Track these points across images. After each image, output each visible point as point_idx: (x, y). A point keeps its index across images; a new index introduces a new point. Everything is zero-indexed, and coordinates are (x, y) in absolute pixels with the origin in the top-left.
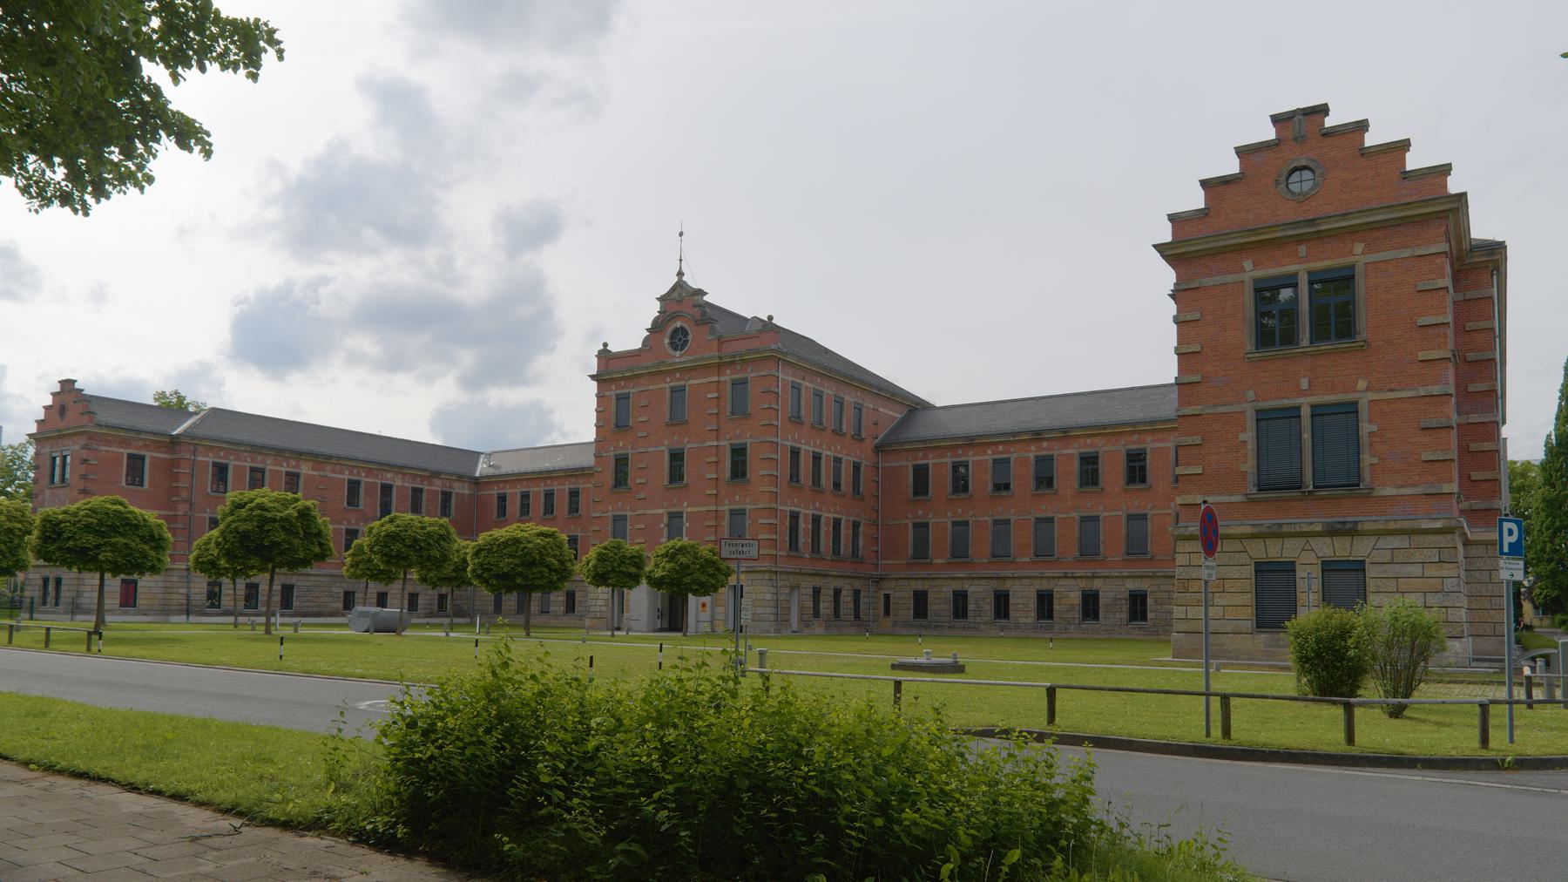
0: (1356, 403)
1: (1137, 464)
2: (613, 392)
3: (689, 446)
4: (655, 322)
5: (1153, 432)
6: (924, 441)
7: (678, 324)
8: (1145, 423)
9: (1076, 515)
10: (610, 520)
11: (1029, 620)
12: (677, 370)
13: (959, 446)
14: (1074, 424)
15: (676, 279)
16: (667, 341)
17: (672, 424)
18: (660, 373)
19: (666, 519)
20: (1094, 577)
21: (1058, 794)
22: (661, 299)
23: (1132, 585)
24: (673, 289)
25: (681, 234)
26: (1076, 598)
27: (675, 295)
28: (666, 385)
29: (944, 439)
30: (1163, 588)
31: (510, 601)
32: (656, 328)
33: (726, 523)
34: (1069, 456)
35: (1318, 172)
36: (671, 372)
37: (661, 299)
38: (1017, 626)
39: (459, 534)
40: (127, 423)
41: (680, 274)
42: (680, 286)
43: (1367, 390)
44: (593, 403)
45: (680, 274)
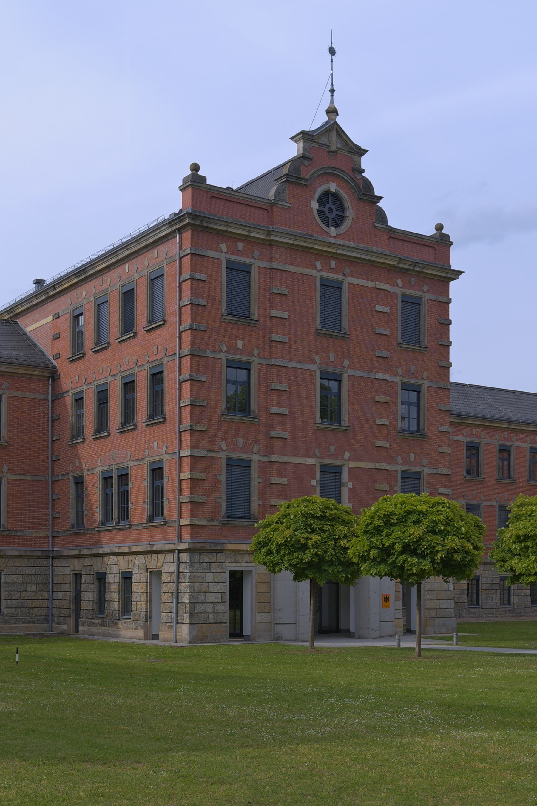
2: (222, 253)
7: (333, 187)
28: (318, 272)
41: (332, 112)
43: (350, 459)
45: (332, 112)
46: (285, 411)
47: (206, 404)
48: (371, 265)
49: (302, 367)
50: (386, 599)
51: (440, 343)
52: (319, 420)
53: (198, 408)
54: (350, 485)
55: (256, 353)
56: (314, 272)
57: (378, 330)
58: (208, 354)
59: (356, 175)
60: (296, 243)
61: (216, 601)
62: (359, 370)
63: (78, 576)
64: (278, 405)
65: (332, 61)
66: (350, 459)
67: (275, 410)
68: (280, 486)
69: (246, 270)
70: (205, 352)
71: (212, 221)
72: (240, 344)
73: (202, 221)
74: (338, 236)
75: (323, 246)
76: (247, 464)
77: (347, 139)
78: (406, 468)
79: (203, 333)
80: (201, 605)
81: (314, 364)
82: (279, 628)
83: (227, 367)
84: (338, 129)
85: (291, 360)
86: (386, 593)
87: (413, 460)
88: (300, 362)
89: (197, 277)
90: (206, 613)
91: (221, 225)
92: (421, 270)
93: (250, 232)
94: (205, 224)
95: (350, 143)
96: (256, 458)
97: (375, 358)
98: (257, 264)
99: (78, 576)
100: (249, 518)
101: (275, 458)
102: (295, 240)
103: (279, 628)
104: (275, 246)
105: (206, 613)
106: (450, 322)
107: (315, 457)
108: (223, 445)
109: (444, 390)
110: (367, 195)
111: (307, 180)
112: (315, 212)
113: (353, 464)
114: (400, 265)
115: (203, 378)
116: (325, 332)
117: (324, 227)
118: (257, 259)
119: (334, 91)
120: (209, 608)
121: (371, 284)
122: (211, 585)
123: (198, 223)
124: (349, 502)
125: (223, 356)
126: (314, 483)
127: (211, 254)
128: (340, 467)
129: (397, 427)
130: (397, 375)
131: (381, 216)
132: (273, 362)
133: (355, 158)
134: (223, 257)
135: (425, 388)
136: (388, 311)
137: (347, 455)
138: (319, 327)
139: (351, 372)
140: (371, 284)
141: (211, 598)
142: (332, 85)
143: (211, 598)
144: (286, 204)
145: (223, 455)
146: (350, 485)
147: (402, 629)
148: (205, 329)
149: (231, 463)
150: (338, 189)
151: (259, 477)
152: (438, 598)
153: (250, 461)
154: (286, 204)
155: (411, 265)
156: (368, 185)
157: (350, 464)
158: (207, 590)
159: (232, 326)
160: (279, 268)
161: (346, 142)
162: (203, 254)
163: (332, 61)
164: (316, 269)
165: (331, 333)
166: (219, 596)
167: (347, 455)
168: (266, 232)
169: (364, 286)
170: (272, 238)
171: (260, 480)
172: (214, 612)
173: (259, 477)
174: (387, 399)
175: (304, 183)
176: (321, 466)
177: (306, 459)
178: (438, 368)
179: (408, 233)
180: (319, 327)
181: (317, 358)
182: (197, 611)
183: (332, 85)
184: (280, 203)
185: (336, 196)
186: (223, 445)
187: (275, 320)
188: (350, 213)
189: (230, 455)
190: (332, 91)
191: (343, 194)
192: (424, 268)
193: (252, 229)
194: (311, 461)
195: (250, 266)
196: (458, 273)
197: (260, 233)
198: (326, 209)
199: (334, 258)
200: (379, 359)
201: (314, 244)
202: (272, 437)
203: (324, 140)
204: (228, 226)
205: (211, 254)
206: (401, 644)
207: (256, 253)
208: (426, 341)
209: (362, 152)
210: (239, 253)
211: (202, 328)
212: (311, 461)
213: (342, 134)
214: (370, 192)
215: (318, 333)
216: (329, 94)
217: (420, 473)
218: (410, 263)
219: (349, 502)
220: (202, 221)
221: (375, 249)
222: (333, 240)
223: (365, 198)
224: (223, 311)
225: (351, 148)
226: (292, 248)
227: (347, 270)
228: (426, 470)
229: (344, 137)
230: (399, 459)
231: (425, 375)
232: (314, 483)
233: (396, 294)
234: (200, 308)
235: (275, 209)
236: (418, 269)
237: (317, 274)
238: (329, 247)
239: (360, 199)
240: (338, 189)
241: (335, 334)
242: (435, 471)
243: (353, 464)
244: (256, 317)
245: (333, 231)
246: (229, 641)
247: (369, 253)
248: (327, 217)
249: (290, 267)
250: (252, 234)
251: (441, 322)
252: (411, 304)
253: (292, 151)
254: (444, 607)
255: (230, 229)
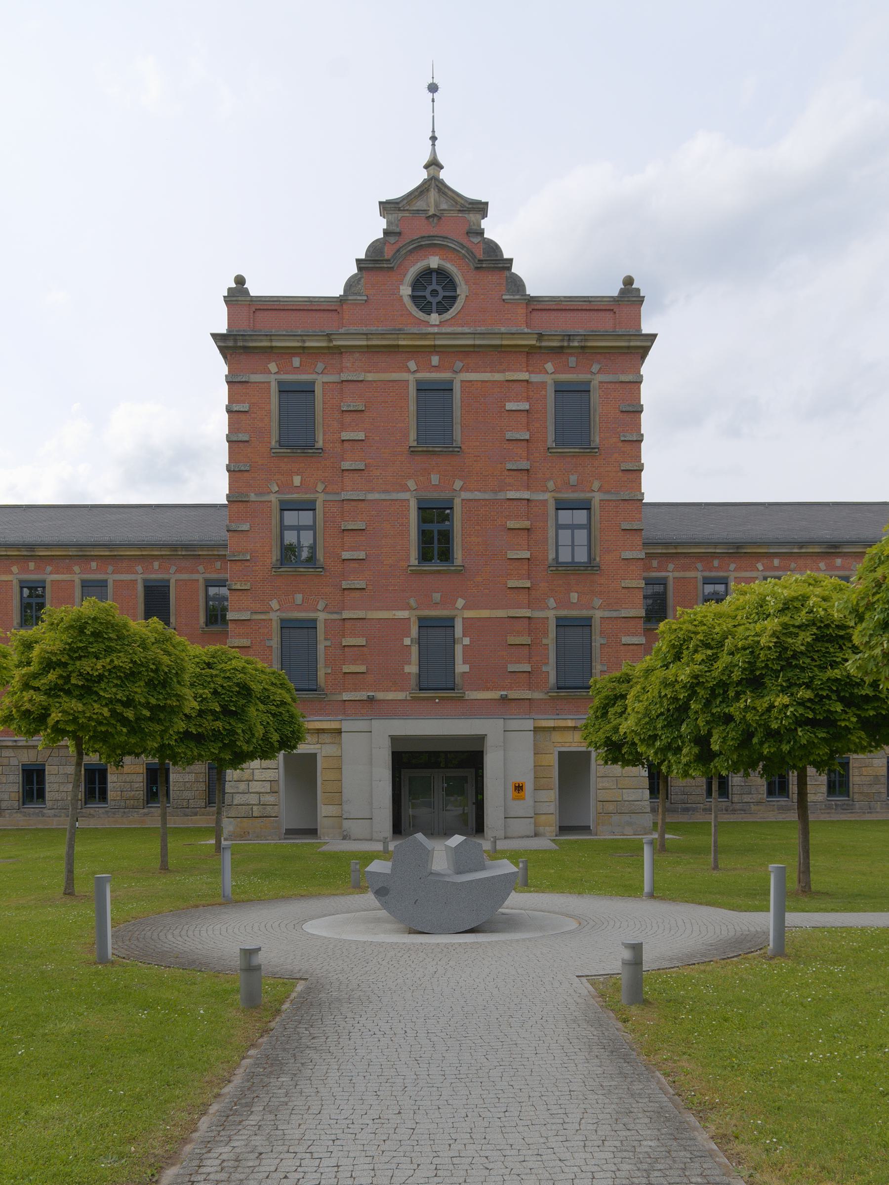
0: (590, 618)
2: (272, 375)
3: (463, 496)
4: (375, 248)
6: (666, 544)
7: (434, 262)
10: (275, 626)
12: (434, 349)
13: (714, 555)
14: (847, 537)
15: (424, 175)
16: (406, 291)
18: (394, 349)
19: (414, 631)
22: (386, 207)
24: (421, 191)
25: (433, 88)
27: (420, 204)
28: (411, 374)
29: (698, 544)
31: (127, 776)
32: (374, 263)
33: (550, 640)
36: (415, 351)
37: (386, 207)
41: (434, 164)
42: (433, 184)
43: (465, 608)
44: (222, 394)
45: (434, 164)
46: (362, 555)
47: (248, 558)
48: (499, 352)
49: (387, 498)
50: (519, 788)
51: (622, 439)
52: (414, 561)
53: (239, 564)
54: (407, 641)
55: (320, 487)
56: (404, 376)
57: (509, 435)
58: (253, 497)
59: (472, 239)
60: (370, 343)
61: (263, 790)
62: (480, 491)
65: (433, 101)
66: (465, 608)
67: (346, 555)
68: (356, 649)
69: (308, 390)
70: (247, 496)
71: (247, 338)
72: (297, 480)
73: (235, 340)
74: (442, 324)
75: (412, 339)
76: (310, 625)
77: (454, 195)
78: (563, 613)
79: (245, 474)
80: (241, 795)
81: (407, 491)
82: (346, 824)
83: (557, 509)
84: (440, 185)
85: (372, 490)
86: (519, 780)
87: (575, 601)
88: (385, 491)
89: (235, 409)
90: (248, 805)
91: (261, 341)
92: (583, 344)
93: (304, 341)
94: (240, 344)
95: (459, 199)
96: (322, 616)
97: (507, 473)
98: (321, 378)
100: (454, 689)
101: (346, 615)
102: (368, 339)
103: (346, 824)
104: (346, 352)
105: (248, 805)
106: (639, 410)
107: (409, 608)
108: (275, 604)
109: (631, 502)
110: (494, 262)
111: (389, 260)
112: (408, 301)
113: (469, 614)
114: (544, 344)
115: (245, 527)
116: (420, 449)
117: (421, 315)
118: (322, 373)
119: (430, 138)
120: (253, 799)
121: (498, 377)
122: (256, 771)
123: (231, 344)
124: (464, 663)
125: (273, 498)
126: (407, 641)
127: (255, 378)
128: (452, 619)
129: (547, 560)
130: (546, 490)
131: (517, 284)
132: (344, 496)
133: (472, 217)
134: (549, 379)
135: (596, 504)
136: (527, 407)
137: (460, 603)
138: (415, 444)
139: (465, 495)
140: (498, 377)
141: (255, 787)
142: (433, 131)
143: (255, 787)
144: (359, 298)
145: (274, 616)
146: (467, 641)
147: (553, 828)
148: (247, 468)
149: (287, 625)
150: (442, 262)
151: (326, 639)
152: (619, 786)
153: (315, 621)
154: (359, 298)
155: (563, 340)
156: (493, 248)
157: (463, 612)
158: (251, 778)
159: (285, 460)
160: (350, 378)
161: (453, 199)
162: (243, 380)
163: (433, 101)
164: (409, 371)
165: (431, 449)
166: (268, 785)
167: (460, 603)
168: (326, 338)
169: (487, 382)
170: (335, 343)
171: (328, 643)
172: (259, 804)
173: (326, 639)
174: (526, 524)
175: (385, 266)
176: (421, 619)
177: (394, 612)
178: (620, 474)
179: (563, 299)
180: (415, 444)
181: (411, 484)
182: (235, 802)
183: (433, 131)
184: (350, 298)
185: (441, 273)
186: (275, 604)
187: (346, 444)
188: (462, 290)
189: (284, 615)
190: (434, 138)
192: (586, 340)
193: (305, 338)
196: (653, 337)
197: (359, 339)
199: (437, 353)
200: (512, 473)
201: (398, 339)
202: (344, 589)
203: (420, 204)
204: (271, 340)
205: (255, 378)
206: (213, 842)
208: (597, 440)
209: (481, 208)
210: (296, 370)
211: (243, 468)
213: (446, 190)
214: (497, 256)
215: (413, 452)
216: (430, 142)
217: (590, 618)
218: (560, 338)
219: (464, 663)
220: (235, 340)
221: (503, 330)
222: (436, 330)
223: (484, 265)
224: (273, 443)
225: (462, 206)
226: (370, 350)
227: (459, 365)
228: (598, 614)
229: (450, 193)
230: (552, 602)
231: (596, 485)
233: (543, 384)
234: (241, 445)
235: (345, 307)
236: (576, 344)
237: (411, 378)
238: (421, 339)
239: (477, 268)
240: (442, 262)
241: (437, 449)
242: (615, 614)
243: (469, 614)
244: (320, 444)
245: (434, 318)
246: (285, 839)
247: (515, 336)
248: (429, 302)
249: (368, 374)
250: (307, 344)
251: (624, 410)
252: (573, 394)
253: (376, 227)
254: (631, 799)
255: (274, 344)
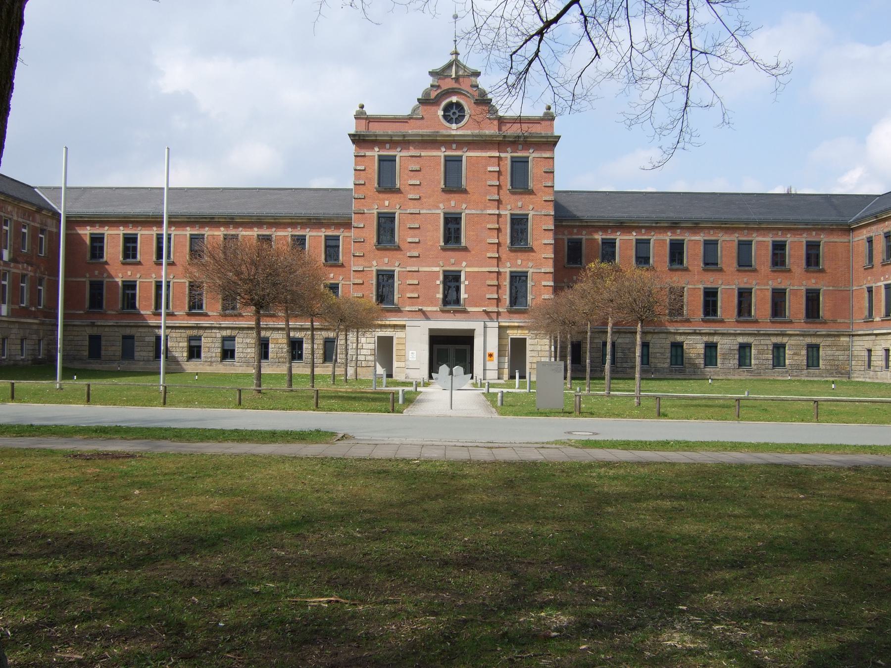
1: (131, 245)
2: (375, 153)
5: (758, 230)
7: (454, 99)
8: (755, 222)
9: (701, 286)
11: (666, 365)
12: (454, 142)
16: (441, 113)
17: (448, 190)
20: (715, 334)
21: (253, 308)
23: (741, 340)
26: (700, 348)
30: (762, 342)
34: (697, 241)
35: (407, 172)
38: (657, 370)
39: (60, 214)
40: (653, 383)
63: (870, 241)
64: (412, 237)
72: (387, 203)
76: (525, 275)
99: (870, 241)
107: (438, 266)
112: (441, 117)
113: (468, 269)
126: (438, 282)
127: (368, 154)
137: (464, 264)
139: (467, 211)
157: (466, 269)
167: (464, 264)
181: (441, 206)
186: (375, 263)
191: (462, 102)
194: (437, 269)
195: (395, 156)
198: (454, 117)
205: (368, 154)
207: (584, 232)
212: (437, 269)
232: (438, 282)
243: (468, 269)
245: (454, 126)
